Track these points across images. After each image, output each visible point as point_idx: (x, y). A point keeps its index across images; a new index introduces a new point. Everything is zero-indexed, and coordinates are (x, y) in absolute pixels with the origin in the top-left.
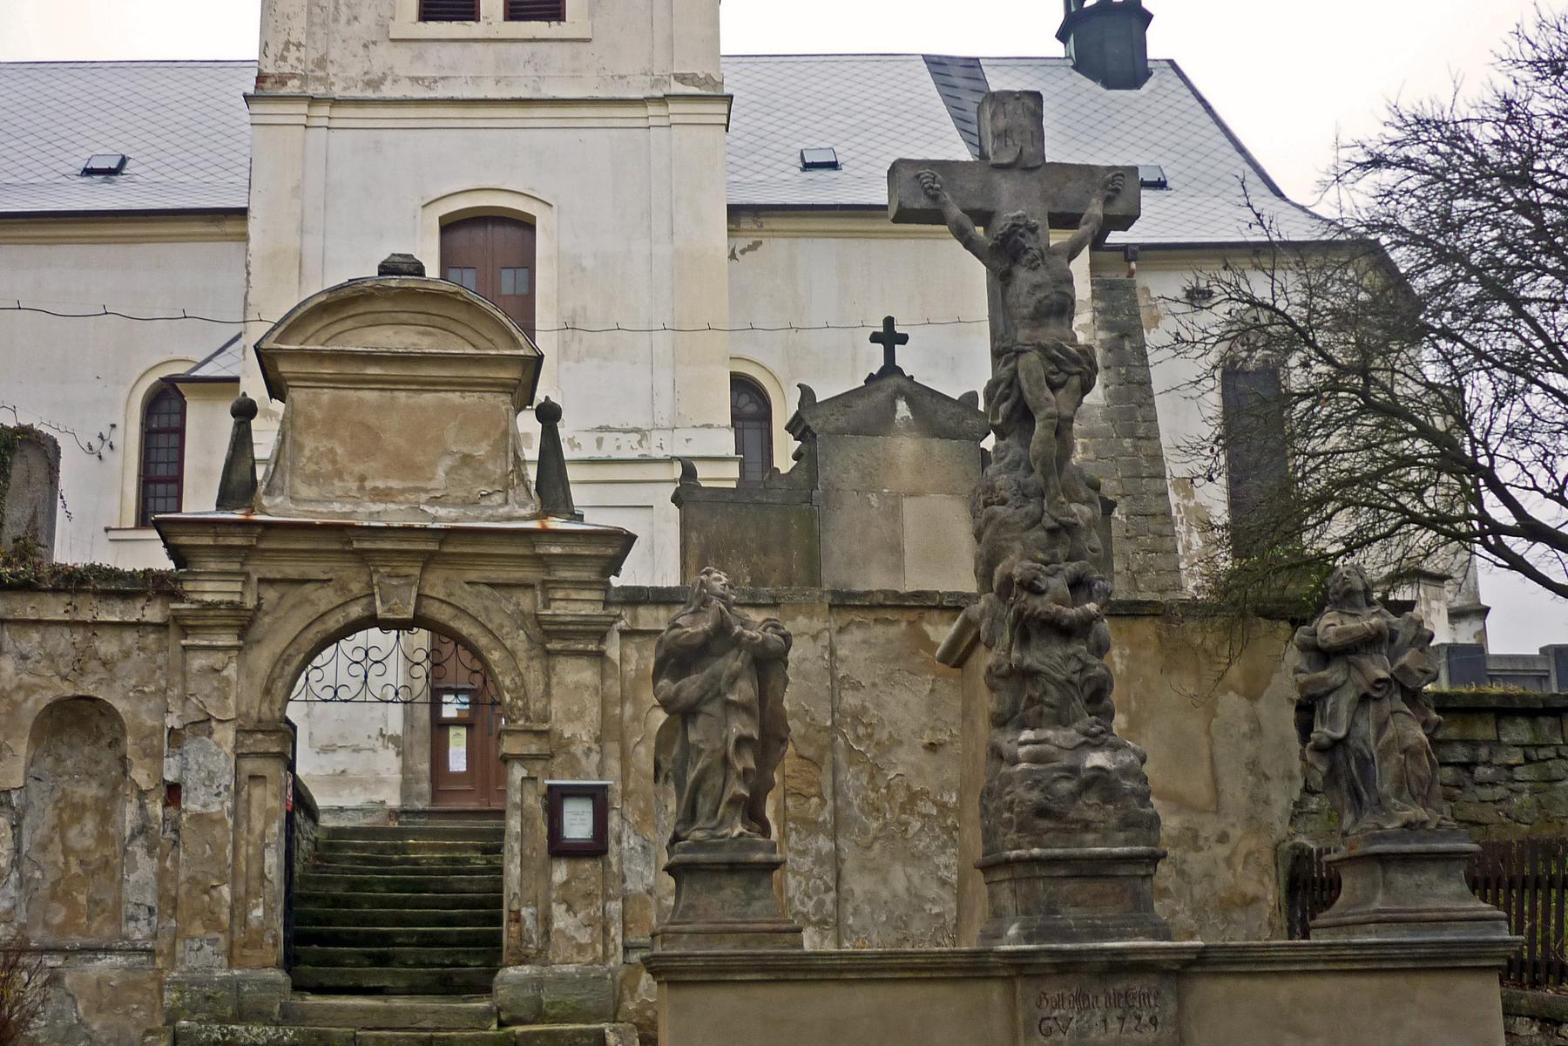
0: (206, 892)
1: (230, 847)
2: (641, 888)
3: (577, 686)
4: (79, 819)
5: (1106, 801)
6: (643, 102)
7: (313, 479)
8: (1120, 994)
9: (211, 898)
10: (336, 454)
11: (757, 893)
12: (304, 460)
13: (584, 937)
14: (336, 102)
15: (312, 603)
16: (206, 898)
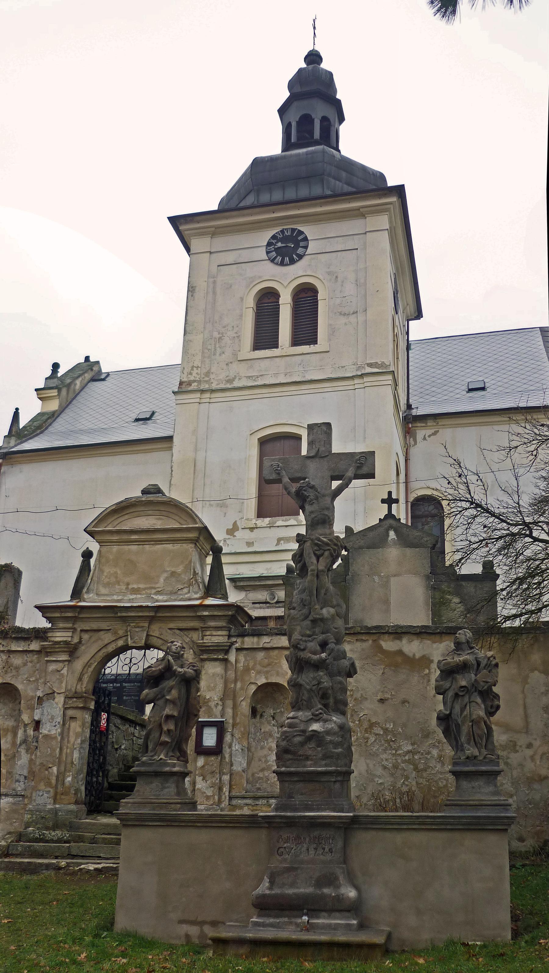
0: (47, 770)
1: (58, 750)
2: (240, 769)
3: (214, 675)
4: (6, 734)
5: (318, 746)
6: (352, 378)
7: (107, 585)
8: (315, 837)
9: (49, 772)
10: (117, 574)
11: (167, 785)
12: (104, 577)
13: (209, 793)
14: (213, 391)
15: (102, 640)
16: (47, 772)
